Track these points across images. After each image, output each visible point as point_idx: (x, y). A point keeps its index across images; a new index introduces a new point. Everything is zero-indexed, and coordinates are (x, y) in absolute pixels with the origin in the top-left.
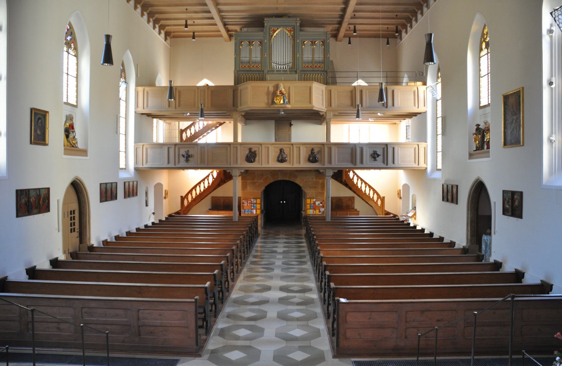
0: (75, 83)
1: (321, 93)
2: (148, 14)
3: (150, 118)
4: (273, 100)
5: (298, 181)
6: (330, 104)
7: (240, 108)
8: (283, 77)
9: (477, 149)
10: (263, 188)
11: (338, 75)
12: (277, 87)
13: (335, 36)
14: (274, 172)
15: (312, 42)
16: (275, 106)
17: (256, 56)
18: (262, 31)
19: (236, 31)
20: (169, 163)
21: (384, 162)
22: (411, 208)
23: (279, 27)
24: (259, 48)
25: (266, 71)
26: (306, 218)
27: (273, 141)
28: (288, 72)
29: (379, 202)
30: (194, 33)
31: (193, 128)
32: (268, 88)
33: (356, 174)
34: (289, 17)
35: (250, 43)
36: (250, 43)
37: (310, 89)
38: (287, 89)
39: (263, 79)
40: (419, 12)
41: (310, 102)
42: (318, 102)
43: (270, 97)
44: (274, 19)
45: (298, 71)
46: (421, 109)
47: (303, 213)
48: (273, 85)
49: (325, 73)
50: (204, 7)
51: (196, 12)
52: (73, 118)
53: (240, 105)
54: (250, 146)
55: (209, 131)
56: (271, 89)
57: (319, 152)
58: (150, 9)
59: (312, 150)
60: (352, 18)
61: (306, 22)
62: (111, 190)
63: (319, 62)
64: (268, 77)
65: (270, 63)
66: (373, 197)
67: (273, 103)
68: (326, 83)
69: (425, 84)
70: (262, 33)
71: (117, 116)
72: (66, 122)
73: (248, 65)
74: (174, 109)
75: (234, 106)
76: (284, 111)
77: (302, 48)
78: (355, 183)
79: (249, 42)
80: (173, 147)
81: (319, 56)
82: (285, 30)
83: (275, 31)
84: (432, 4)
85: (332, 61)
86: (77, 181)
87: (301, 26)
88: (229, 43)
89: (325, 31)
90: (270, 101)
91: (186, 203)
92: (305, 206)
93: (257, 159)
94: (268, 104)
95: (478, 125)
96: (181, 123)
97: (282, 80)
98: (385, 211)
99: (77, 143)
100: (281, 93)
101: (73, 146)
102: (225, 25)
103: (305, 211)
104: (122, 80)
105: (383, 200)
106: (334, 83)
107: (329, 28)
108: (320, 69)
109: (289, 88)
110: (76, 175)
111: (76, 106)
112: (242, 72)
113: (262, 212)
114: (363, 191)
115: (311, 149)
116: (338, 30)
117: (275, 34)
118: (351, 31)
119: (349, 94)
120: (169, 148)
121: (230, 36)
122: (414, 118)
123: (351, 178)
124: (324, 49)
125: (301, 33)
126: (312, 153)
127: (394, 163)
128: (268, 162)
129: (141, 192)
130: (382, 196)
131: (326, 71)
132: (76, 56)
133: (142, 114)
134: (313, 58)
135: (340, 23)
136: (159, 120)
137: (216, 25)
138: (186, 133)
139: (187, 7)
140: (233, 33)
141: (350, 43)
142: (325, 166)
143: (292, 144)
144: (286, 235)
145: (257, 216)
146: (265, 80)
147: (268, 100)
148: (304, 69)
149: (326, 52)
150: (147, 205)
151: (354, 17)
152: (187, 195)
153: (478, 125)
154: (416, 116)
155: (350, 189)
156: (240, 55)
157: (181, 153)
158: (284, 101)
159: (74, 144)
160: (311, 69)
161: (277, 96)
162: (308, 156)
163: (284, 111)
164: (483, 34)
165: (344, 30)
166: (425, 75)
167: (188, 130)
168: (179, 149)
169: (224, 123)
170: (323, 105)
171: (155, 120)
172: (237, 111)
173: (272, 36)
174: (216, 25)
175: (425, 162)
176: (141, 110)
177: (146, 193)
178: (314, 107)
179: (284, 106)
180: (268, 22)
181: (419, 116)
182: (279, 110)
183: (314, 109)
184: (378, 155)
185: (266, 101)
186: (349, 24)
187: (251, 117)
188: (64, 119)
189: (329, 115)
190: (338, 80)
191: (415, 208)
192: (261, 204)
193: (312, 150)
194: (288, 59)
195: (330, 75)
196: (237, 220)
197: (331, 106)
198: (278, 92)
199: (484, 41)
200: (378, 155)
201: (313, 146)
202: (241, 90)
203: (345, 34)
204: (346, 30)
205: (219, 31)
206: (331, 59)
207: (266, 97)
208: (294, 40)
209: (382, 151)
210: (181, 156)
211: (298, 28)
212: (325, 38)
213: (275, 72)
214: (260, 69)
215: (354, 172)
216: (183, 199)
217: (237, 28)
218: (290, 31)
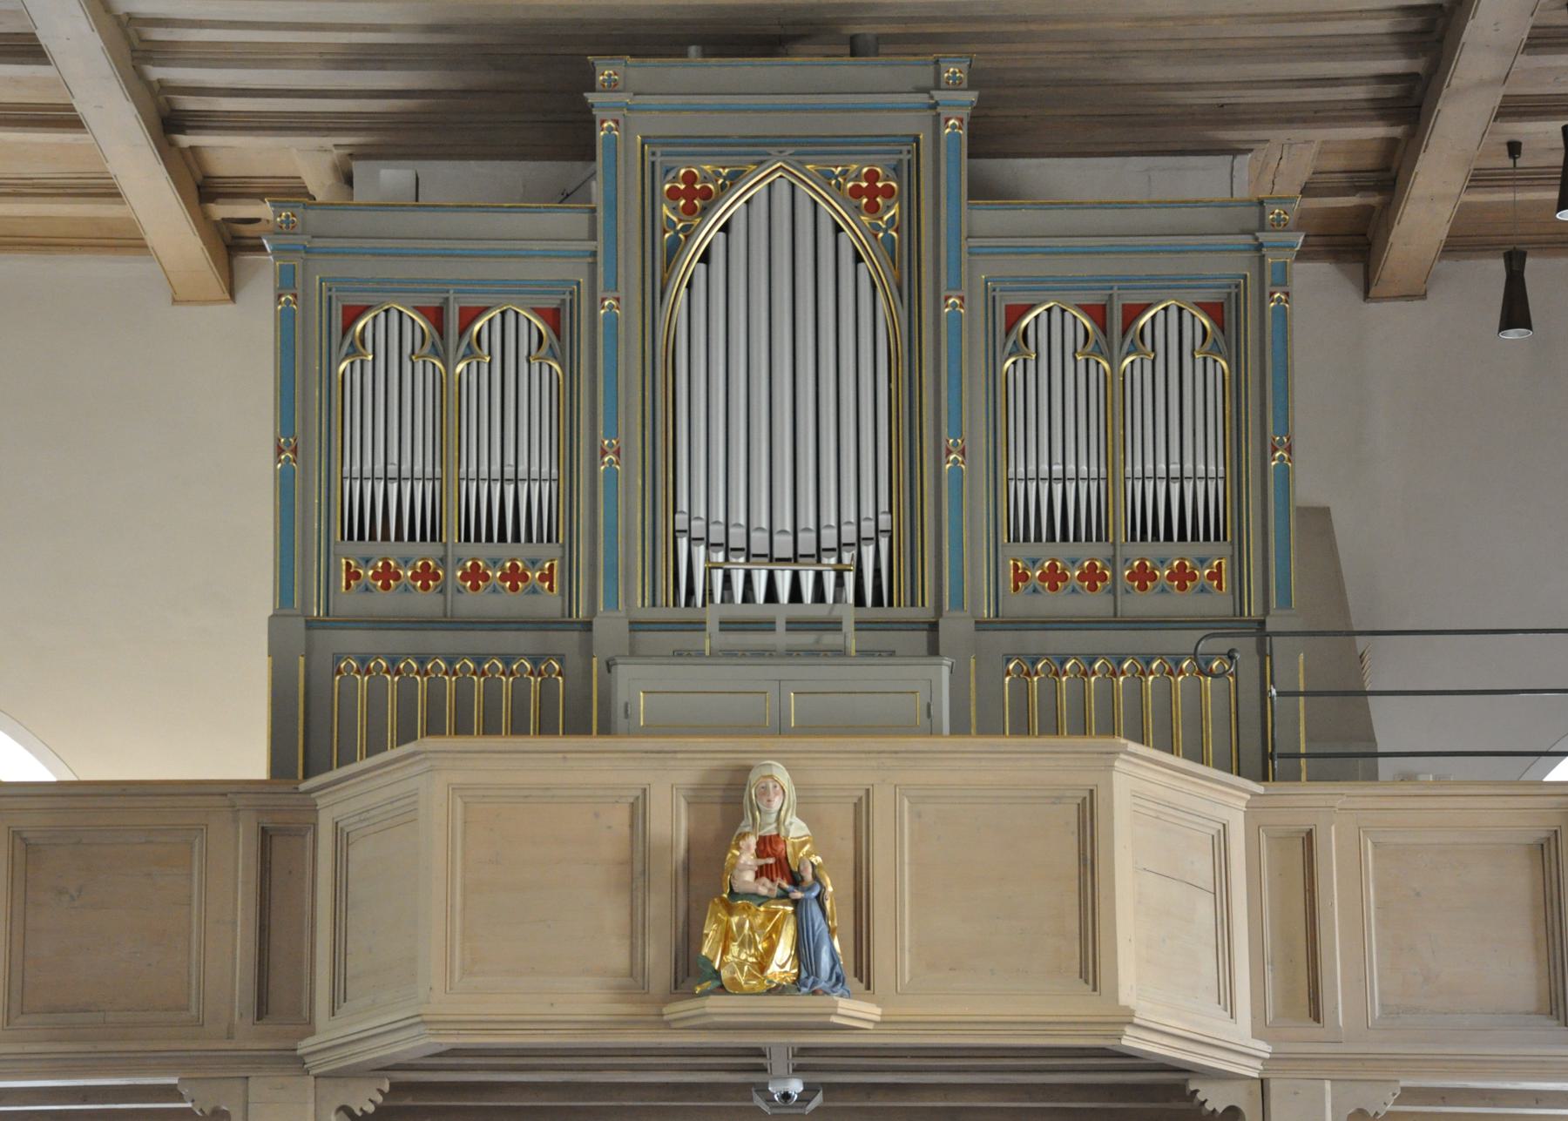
1: (1203, 868)
4: (689, 939)
6: (1302, 982)
7: (329, 1031)
8: (791, 688)
11: (1385, 665)
12: (730, 799)
13: (1355, 243)
15: (1099, 314)
16: (716, 1005)
17: (512, 456)
18: (567, 196)
19: (290, 193)
23: (758, 147)
24: (537, 380)
25: (610, 628)
28: (851, 639)
32: (638, 810)
34: (857, 47)
35: (447, 324)
36: (447, 324)
37: (1088, 818)
38: (843, 819)
39: (580, 713)
41: (1091, 963)
43: (661, 906)
44: (696, 70)
45: (954, 627)
48: (688, 773)
49: (1246, 646)
53: (338, 998)
56: (672, 824)
63: (1175, 530)
64: (637, 687)
65: (662, 535)
67: (691, 972)
68: (1262, 759)
70: (570, 221)
75: (262, 1009)
76: (805, 1060)
79: (436, 316)
81: (1177, 457)
83: (710, 200)
85: (1320, 517)
87: (986, 138)
89: (1242, 192)
90: (659, 957)
94: (634, 982)
97: (781, 729)
100: (776, 863)
102: (169, 122)
106: (1350, 757)
107: (1288, 164)
108: (1188, 603)
109: (862, 810)
112: (360, 640)
116: (1387, 177)
117: (707, 232)
118: (1533, 178)
119: (1520, 882)
121: (231, 246)
124: (1235, 387)
125: (988, 218)
131: (1260, 628)
134: (1108, 480)
135: (1410, 105)
137: (66, 119)
140: (263, 210)
141: (1515, 313)
146: (606, 729)
147: (636, 932)
148: (1018, 604)
149: (1254, 413)
156: (332, 448)
158: (804, 952)
160: (1096, 604)
161: (734, 899)
163: (805, 1060)
165: (1457, 178)
170: (1227, 1001)
172: (298, 1063)
173: (674, 251)
174: (66, 119)
178: (1127, 1019)
179: (801, 1005)
180: (630, 104)
182: (754, 1060)
183: (1130, 1040)
185: (617, 956)
186: (1512, 109)
190: (1392, 724)
194: (851, 499)
195: (1296, 665)
197: (1316, 1015)
198: (746, 857)
202: (342, 839)
203: (1464, 211)
204: (1479, 179)
205: (111, 193)
206: (1306, 491)
207: (614, 914)
208: (908, 290)
211: (956, 168)
212: (1240, 265)
213: (712, 639)
214: (550, 604)
217: (307, 161)
218: (868, 196)
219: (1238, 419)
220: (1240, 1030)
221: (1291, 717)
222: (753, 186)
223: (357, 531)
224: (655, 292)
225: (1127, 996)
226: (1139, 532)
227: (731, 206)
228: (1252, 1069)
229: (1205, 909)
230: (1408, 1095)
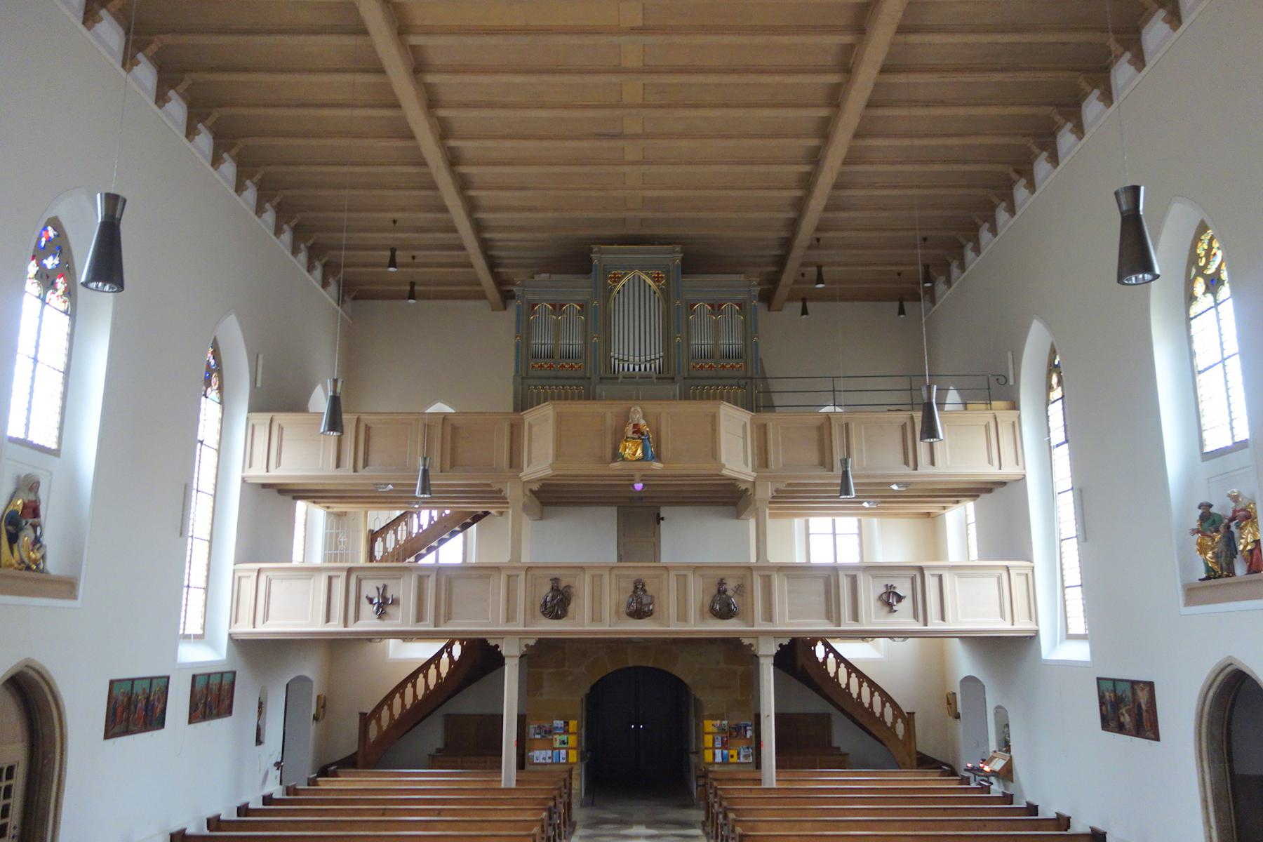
0: (60, 388)
1: (740, 431)
2: (324, 266)
3: (286, 499)
4: (616, 448)
5: (681, 669)
6: (763, 460)
9: (1211, 575)
10: (587, 690)
12: (626, 417)
14: (615, 645)
17: (574, 342)
20: (328, 620)
21: (915, 617)
22: (993, 745)
26: (705, 776)
27: (612, 558)
29: (900, 728)
30: (393, 251)
31: (402, 529)
33: (832, 650)
35: (557, 308)
40: (970, 245)
42: (735, 460)
46: (1009, 470)
47: (693, 758)
50: (439, 216)
51: (419, 230)
52: (38, 483)
54: (556, 573)
55: (446, 536)
56: (610, 420)
57: (740, 589)
58: (216, 114)
59: (721, 582)
60: (810, 247)
61: (698, 259)
62: (148, 698)
66: (882, 714)
67: (616, 456)
68: (750, 404)
69: (1015, 406)
71: (186, 486)
72: (13, 497)
73: (551, 362)
74: (351, 473)
76: (643, 479)
77: (688, 322)
78: (832, 675)
80: (344, 574)
81: (732, 341)
82: (644, 277)
83: (620, 279)
84: (944, 293)
86: (32, 673)
88: (502, 314)
91: (373, 733)
92: (700, 738)
93: (572, 607)
95: (1206, 507)
96: (372, 514)
98: (918, 753)
99: (43, 557)
100: (637, 430)
101: (28, 568)
103: (699, 752)
104: (213, 394)
105: (909, 719)
106: (771, 407)
110: (32, 656)
111: (56, 453)
113: (582, 757)
114: (855, 696)
115: (717, 580)
117: (619, 286)
120: (330, 579)
122: (985, 497)
123: (821, 660)
124: (745, 322)
126: (719, 591)
127: (943, 619)
128: (596, 617)
129: (244, 700)
130: (906, 709)
132: (72, 314)
133: (264, 486)
136: (312, 506)
138: (384, 540)
139: (415, 253)
141: (805, 312)
142: (756, 628)
143: (666, 568)
144: (649, 825)
145: (570, 771)
146: (594, 399)
149: (749, 330)
150: (259, 741)
151: (817, 243)
152: (379, 708)
153: (1206, 507)
154: (990, 491)
155: (818, 689)
157: (364, 593)
158: (644, 451)
159: (35, 562)
160: (713, 373)
162: (708, 600)
164: (1193, 258)
166: (1011, 382)
167: (391, 532)
168: (359, 582)
169: (486, 513)
171: (301, 506)
173: (611, 290)
175: (1032, 614)
176: (258, 472)
177: (261, 705)
180: (599, 257)
181: (998, 491)
182: (631, 478)
183: (724, 472)
184: (900, 598)
187: (552, 498)
188: (9, 488)
189: (765, 492)
191: (1006, 745)
192: (578, 734)
193: (721, 582)
194: (654, 351)
196: (513, 785)
198: (630, 429)
199: (1201, 272)
200: (900, 598)
201: (721, 573)
202: (530, 426)
205: (471, 266)
209: (908, 585)
210: (364, 602)
215: (827, 645)
216: (365, 719)
218: (656, 279)
219: (337, 802)
220: (749, 470)
221: (756, 397)
222: (630, 276)
223: (535, 356)
224: (606, 299)
225: (723, 461)
226: (722, 357)
227: (624, 281)
228: (751, 479)
229: (741, 442)
230: (789, 485)
